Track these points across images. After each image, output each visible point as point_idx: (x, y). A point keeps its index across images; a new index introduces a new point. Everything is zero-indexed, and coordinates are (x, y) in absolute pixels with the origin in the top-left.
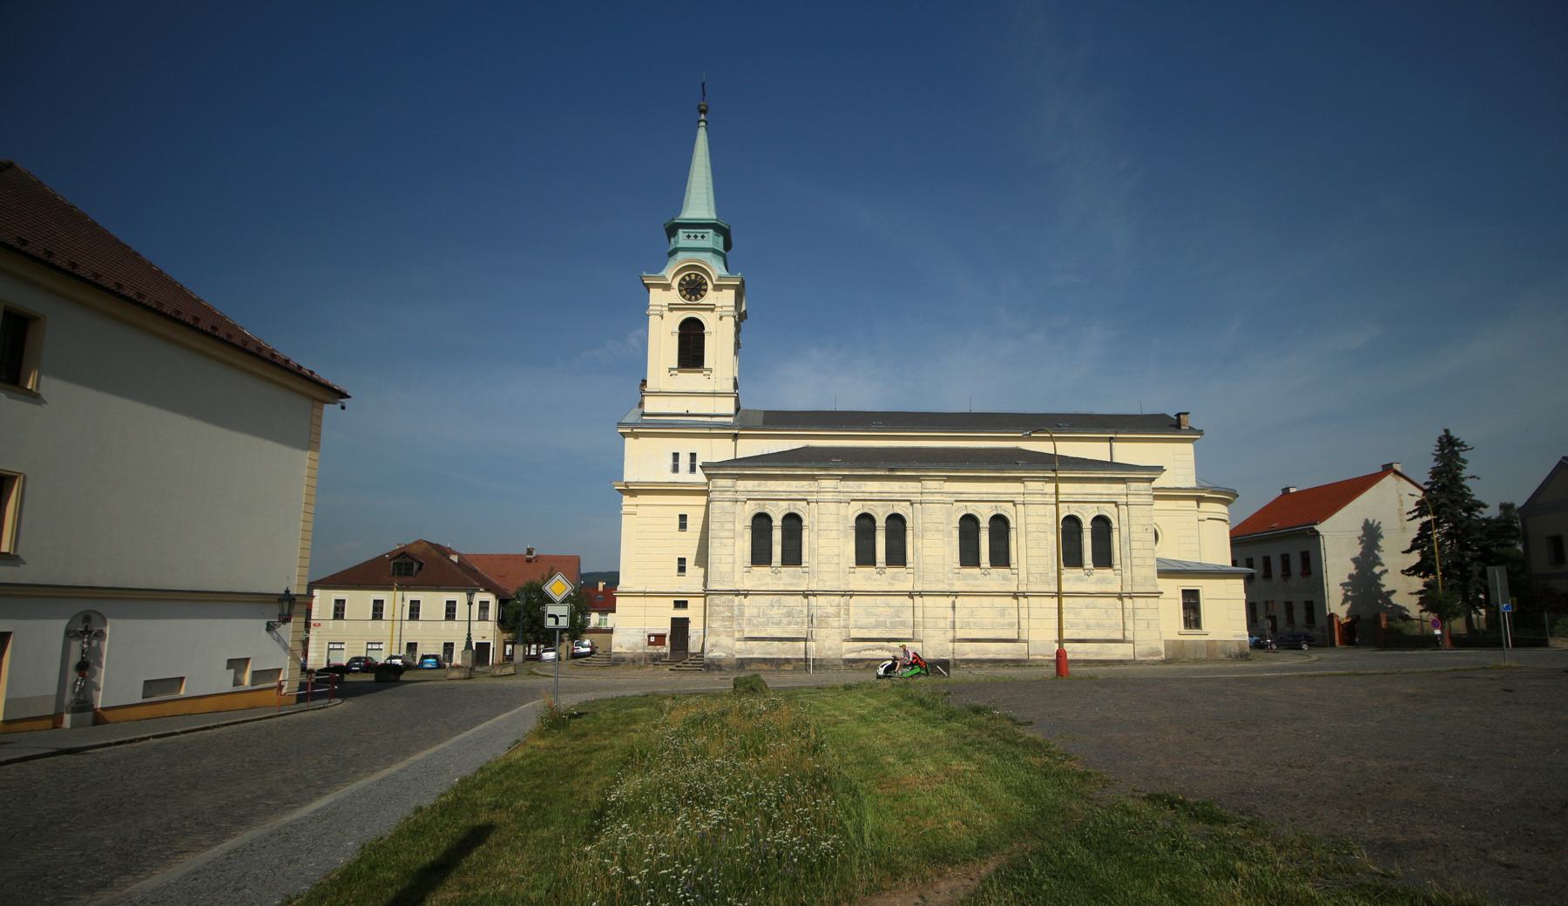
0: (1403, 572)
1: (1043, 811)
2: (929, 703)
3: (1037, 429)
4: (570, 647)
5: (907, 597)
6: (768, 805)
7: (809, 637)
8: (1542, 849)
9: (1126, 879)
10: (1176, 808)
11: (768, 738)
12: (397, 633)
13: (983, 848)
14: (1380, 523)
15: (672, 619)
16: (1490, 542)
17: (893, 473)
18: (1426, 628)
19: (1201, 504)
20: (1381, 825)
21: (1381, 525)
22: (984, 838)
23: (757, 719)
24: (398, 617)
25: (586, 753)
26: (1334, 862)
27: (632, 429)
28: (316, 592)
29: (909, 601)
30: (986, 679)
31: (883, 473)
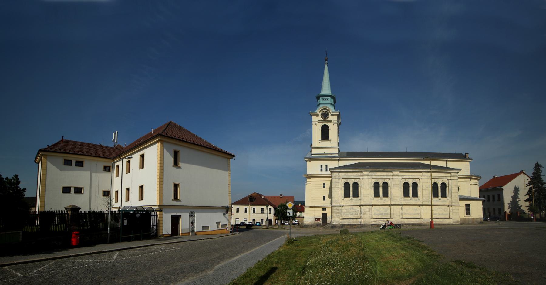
0: (524, 201)
3: (426, 157)
4: (292, 222)
5: (389, 206)
6: (350, 265)
7: (361, 218)
11: (350, 246)
13: (410, 276)
18: (529, 216)
23: (347, 241)
24: (250, 212)
25: (299, 251)
28: (233, 206)
31: (381, 170)
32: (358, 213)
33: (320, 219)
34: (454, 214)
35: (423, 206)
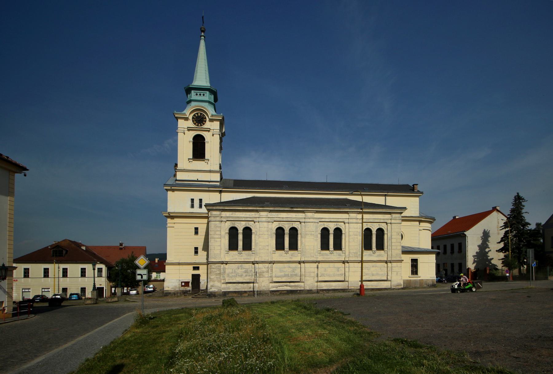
0: (497, 251)
1: (354, 347)
2: (308, 308)
6: (245, 350)
7: (255, 281)
8: (529, 352)
9: (384, 369)
10: (404, 343)
12: (57, 283)
13: (331, 361)
14: (489, 231)
15: (192, 274)
16: (530, 239)
17: (293, 209)
18: (503, 273)
19: (421, 223)
20: (476, 346)
21: (490, 232)
22: (332, 357)
24: (57, 276)
25: (160, 334)
26: (458, 359)
27: (171, 187)
29: (298, 265)
30: (331, 297)
31: (288, 209)
32: (250, 274)
33: (188, 282)
34: (394, 274)
35: (349, 263)
